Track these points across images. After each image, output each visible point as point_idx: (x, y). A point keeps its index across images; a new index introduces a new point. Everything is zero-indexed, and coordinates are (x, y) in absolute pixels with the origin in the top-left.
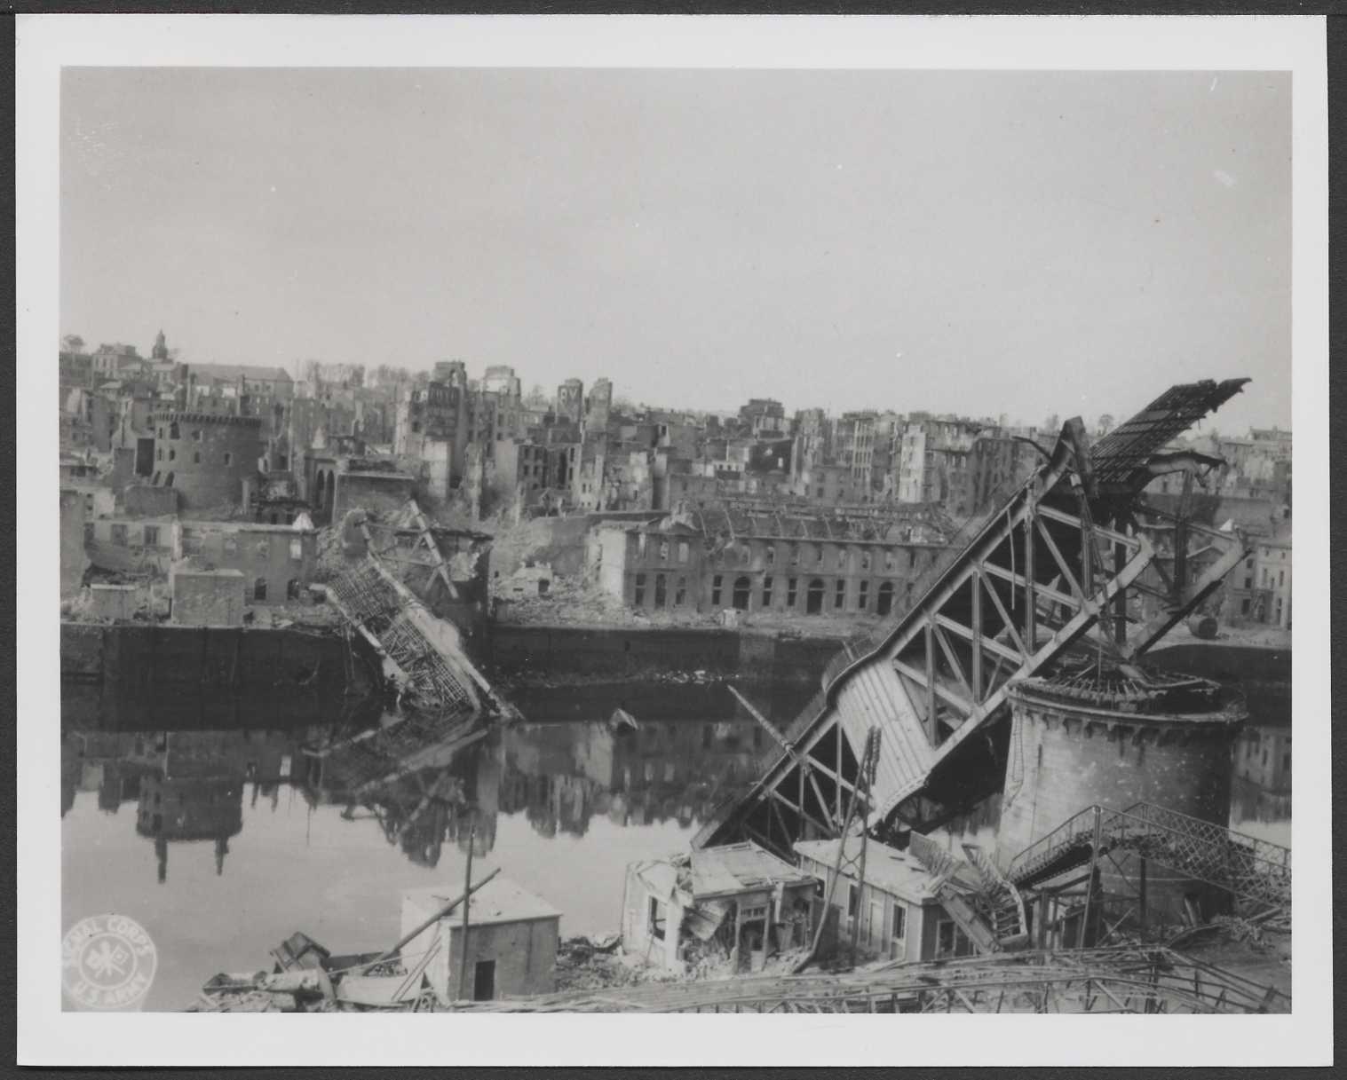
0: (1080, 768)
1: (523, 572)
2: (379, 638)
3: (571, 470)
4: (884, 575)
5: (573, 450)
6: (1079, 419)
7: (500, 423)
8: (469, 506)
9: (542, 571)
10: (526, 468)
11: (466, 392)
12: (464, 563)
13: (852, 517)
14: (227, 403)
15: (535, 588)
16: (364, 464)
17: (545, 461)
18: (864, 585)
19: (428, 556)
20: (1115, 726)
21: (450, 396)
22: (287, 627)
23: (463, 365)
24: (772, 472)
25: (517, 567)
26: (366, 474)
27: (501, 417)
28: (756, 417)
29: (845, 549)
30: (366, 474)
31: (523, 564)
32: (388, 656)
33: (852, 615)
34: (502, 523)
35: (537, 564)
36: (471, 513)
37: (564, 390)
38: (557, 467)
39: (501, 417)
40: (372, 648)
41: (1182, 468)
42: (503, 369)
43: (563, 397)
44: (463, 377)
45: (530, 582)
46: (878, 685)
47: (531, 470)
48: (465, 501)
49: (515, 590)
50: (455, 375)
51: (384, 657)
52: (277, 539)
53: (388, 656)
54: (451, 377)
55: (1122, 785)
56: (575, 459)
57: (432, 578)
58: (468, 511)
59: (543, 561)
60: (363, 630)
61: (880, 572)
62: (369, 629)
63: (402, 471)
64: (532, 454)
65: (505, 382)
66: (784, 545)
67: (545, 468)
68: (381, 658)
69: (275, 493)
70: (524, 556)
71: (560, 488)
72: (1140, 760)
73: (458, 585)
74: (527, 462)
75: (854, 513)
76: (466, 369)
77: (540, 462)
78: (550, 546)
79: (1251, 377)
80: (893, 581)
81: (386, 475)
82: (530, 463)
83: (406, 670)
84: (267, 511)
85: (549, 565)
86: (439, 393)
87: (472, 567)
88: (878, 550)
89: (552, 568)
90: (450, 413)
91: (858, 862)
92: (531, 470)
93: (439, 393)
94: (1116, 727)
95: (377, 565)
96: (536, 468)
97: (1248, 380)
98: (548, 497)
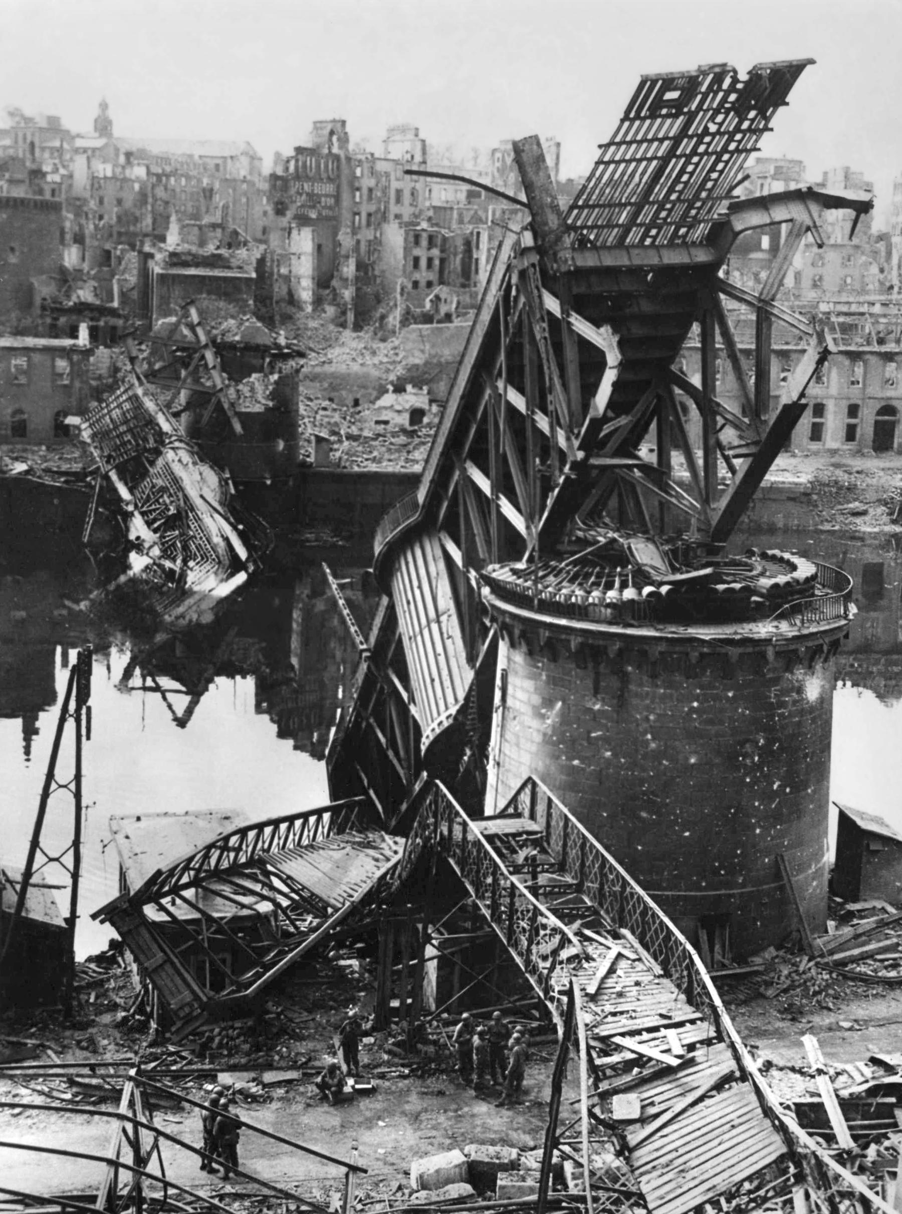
0: (543, 711)
1: (388, 399)
2: (131, 490)
3: (477, 260)
4: (880, 395)
5: (478, 234)
6: (535, 140)
7: (398, 200)
8: (344, 313)
9: (414, 398)
10: (416, 260)
11: (349, 159)
12: (259, 388)
13: (839, 314)
14: (137, 186)
15: (404, 420)
16: (189, 258)
17: (442, 251)
18: (853, 410)
19: (209, 379)
20: (582, 644)
21: (326, 166)
22: (20, 473)
23: (344, 123)
24: (754, 255)
25: (383, 391)
26: (192, 271)
27: (399, 192)
28: (760, 182)
29: (861, 359)
30: (192, 271)
31: (391, 388)
32: (136, 513)
33: (834, 452)
34: (380, 335)
35: (409, 388)
36: (346, 321)
37: (498, 155)
38: (460, 257)
39: (399, 192)
40: (120, 499)
41: (788, 217)
42: (403, 130)
43: (498, 164)
44: (344, 140)
45: (399, 412)
46: (422, 572)
47: (423, 263)
48: (338, 305)
49: (377, 422)
50: (335, 138)
51: (132, 514)
52: (37, 358)
53: (136, 513)
54: (330, 140)
55: (597, 738)
56: (481, 246)
57: (211, 407)
58: (342, 319)
59: (418, 384)
60: (113, 476)
61: (875, 390)
62: (122, 478)
63: (240, 268)
64: (424, 242)
65: (407, 146)
66: (841, 358)
67: (442, 261)
68: (128, 516)
69: (78, 297)
70: (392, 377)
71: (463, 286)
72: (621, 701)
73: (245, 418)
74: (417, 252)
75: (845, 309)
76: (348, 129)
77: (436, 252)
78: (427, 363)
79: (815, 58)
80: (895, 403)
81: (217, 273)
82: (421, 252)
83: (155, 531)
84: (63, 320)
85: (425, 388)
86: (311, 161)
87: (268, 392)
88: (873, 360)
89: (429, 393)
90: (329, 188)
91: (69, 860)
92: (423, 263)
93: (311, 161)
94: (582, 645)
95: (140, 391)
96: (430, 260)
97: (812, 62)
98: (437, 297)
